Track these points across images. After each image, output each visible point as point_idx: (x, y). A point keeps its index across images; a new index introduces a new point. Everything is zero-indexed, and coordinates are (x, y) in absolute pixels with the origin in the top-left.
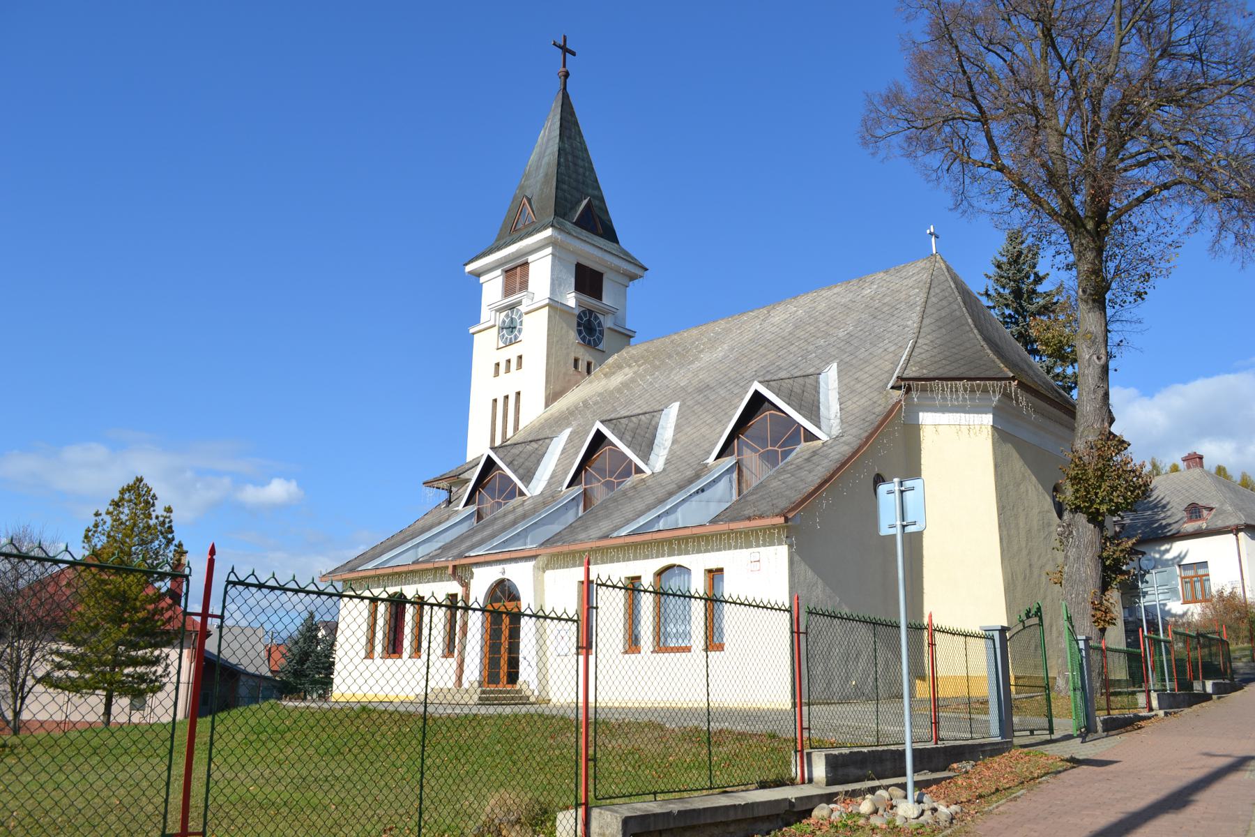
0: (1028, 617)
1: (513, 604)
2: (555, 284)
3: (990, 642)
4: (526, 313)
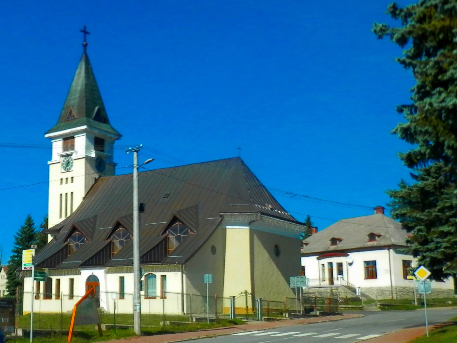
2: (87, 148)
3: (230, 299)
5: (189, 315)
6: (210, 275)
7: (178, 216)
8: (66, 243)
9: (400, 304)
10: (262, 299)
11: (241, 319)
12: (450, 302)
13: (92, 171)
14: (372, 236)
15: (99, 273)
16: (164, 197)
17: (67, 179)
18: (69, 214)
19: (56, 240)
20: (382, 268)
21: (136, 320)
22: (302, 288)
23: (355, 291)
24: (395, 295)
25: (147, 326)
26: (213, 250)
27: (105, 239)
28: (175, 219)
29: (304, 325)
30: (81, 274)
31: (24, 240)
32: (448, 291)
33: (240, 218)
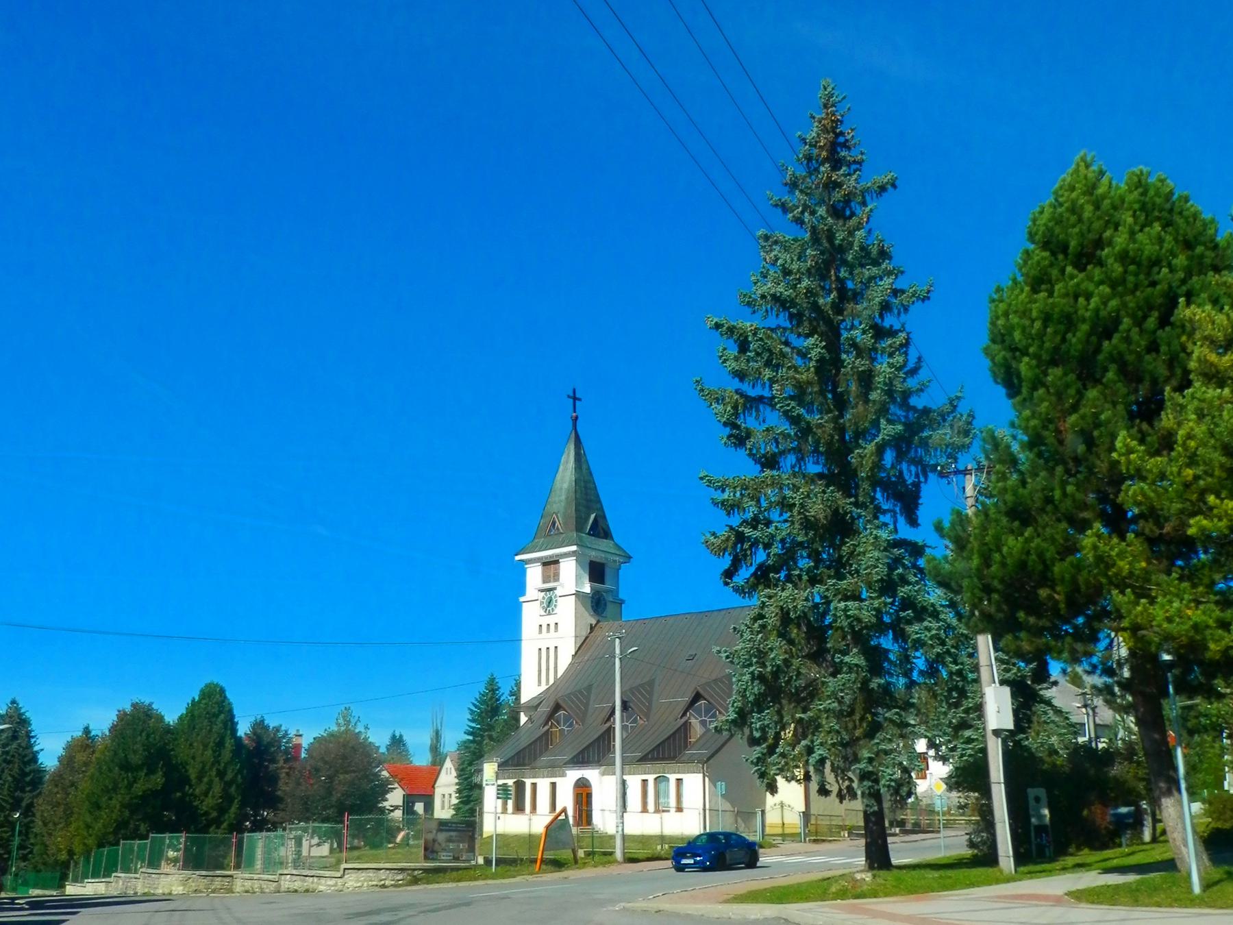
1: (594, 555)
2: (578, 578)
7: (702, 692)
13: (586, 614)
18: (551, 681)
28: (697, 697)
31: (484, 714)
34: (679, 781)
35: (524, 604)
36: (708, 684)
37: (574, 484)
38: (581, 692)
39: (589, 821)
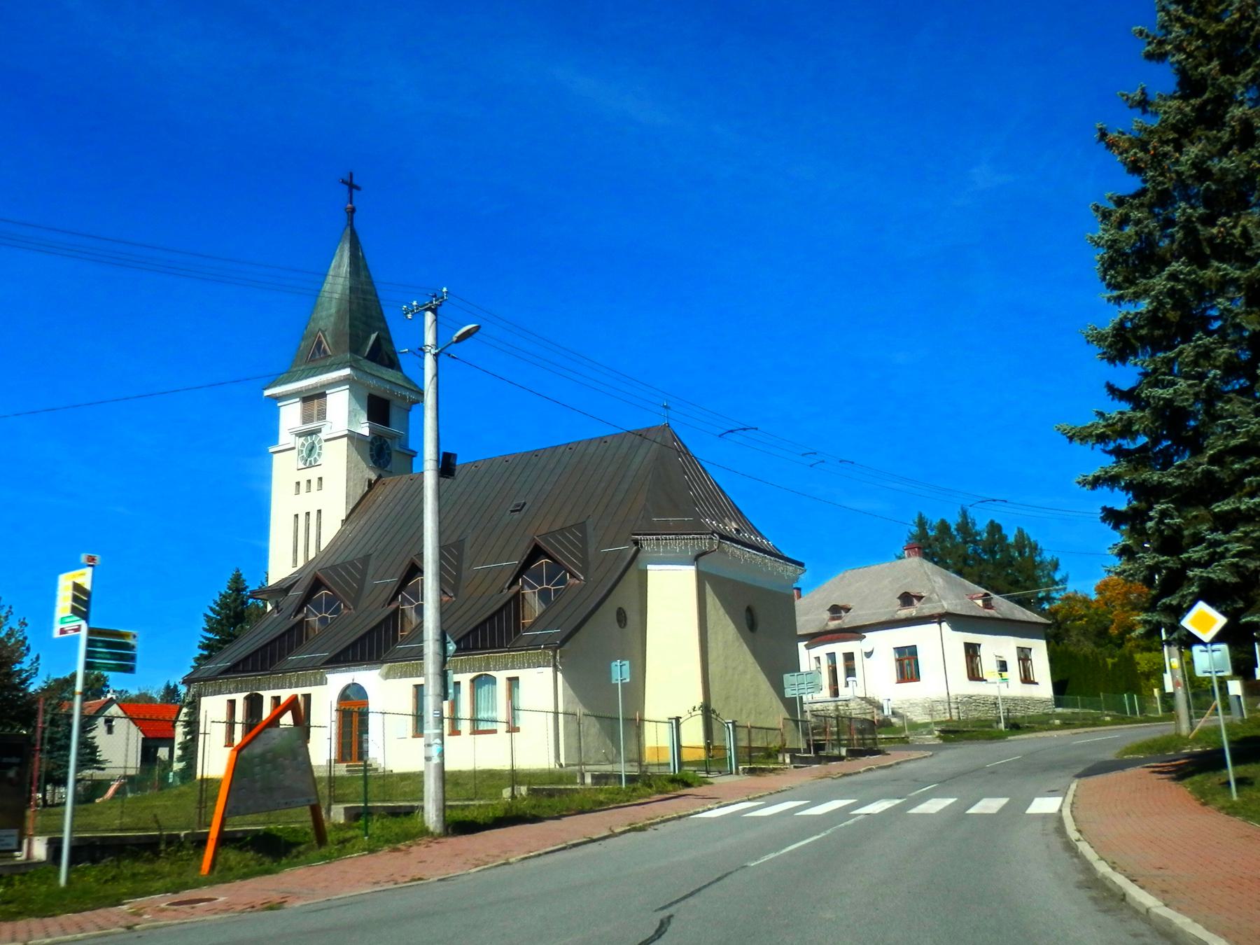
0: (694, 710)
2: (352, 415)
4: (326, 441)
5: (577, 768)
6: (627, 663)
7: (543, 544)
8: (300, 617)
9: (974, 729)
10: (737, 723)
11: (695, 771)
12: (1057, 722)
13: (363, 465)
14: (907, 599)
15: (369, 678)
16: (512, 511)
17: (309, 481)
19: (278, 612)
20: (927, 661)
21: (431, 788)
22: (801, 698)
23: (881, 708)
24: (954, 712)
25: (466, 803)
26: (621, 617)
27: (384, 605)
28: (537, 552)
29: (835, 781)
30: (326, 684)
31: (224, 621)
32: (1042, 702)
33: (677, 546)
34: (513, 681)
35: (275, 456)
36: (552, 534)
37: (348, 292)
38: (352, 563)
39: (362, 754)
